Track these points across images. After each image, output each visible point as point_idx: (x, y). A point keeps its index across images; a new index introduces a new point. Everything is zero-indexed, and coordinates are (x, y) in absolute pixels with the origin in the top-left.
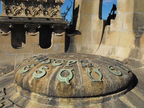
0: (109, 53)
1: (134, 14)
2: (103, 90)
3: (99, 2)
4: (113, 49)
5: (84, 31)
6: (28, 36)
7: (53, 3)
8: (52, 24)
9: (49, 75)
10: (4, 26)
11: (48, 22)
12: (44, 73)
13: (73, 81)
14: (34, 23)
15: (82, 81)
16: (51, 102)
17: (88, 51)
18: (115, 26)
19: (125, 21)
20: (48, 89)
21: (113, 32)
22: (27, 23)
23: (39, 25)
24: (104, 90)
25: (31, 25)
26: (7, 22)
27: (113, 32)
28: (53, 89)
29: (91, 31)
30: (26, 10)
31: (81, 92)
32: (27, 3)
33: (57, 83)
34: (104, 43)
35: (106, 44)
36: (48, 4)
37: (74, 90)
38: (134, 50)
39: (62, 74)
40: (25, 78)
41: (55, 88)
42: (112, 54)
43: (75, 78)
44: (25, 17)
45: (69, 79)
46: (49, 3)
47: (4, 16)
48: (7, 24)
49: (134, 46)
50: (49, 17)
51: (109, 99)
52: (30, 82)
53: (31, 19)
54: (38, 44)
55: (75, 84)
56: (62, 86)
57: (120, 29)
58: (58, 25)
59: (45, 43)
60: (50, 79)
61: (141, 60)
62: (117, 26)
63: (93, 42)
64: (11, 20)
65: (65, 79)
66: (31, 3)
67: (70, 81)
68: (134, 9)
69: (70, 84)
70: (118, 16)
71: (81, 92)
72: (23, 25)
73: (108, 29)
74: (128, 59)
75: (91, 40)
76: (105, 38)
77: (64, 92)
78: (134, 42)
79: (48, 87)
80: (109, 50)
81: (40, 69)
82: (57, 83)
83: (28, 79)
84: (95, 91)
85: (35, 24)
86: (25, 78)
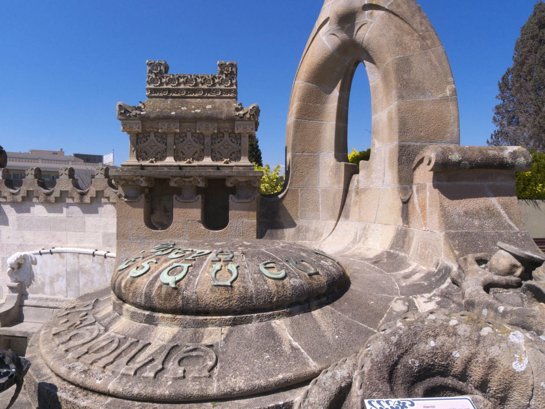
0: (354, 239)
1: (400, 146)
2: (231, 301)
3: (335, 123)
4: (364, 229)
5: (301, 190)
9: (152, 272)
10: (130, 183)
11: (218, 174)
13: (183, 283)
14: (191, 177)
15: (196, 284)
16: (148, 318)
17: (311, 236)
18: (369, 176)
19: (387, 165)
20: (143, 294)
21: (365, 190)
22: (175, 177)
23: (199, 180)
24: (235, 301)
25: (184, 181)
26: (136, 176)
27: (365, 190)
28: (150, 295)
29: (319, 190)
31: (191, 301)
32: (177, 136)
33: (157, 284)
34: (347, 217)
35: (350, 218)
36: (221, 135)
37: (180, 297)
38: (401, 230)
40: (119, 279)
41: (154, 293)
42: (359, 241)
43: (189, 277)
44: (171, 164)
45: (177, 279)
46: (223, 133)
47: (132, 163)
48: (136, 180)
49: (400, 222)
51: (249, 321)
52: (123, 284)
53: (288, 164)
54: (199, 221)
55: (184, 287)
58: (240, 180)
59: (215, 219)
60: (151, 279)
61: (408, 254)
62: (374, 175)
63: (322, 213)
64: (144, 172)
65: (171, 280)
66: (186, 136)
67: (177, 282)
68: (400, 137)
69: (175, 289)
70: (375, 151)
71: (191, 301)
73: (356, 183)
74: (388, 253)
75: (318, 210)
76: (350, 206)
77: (165, 299)
78: (400, 211)
79: (144, 292)
80: (357, 233)
82: (157, 284)
83: (123, 278)
84: (216, 301)
85: (192, 179)
86: (119, 279)
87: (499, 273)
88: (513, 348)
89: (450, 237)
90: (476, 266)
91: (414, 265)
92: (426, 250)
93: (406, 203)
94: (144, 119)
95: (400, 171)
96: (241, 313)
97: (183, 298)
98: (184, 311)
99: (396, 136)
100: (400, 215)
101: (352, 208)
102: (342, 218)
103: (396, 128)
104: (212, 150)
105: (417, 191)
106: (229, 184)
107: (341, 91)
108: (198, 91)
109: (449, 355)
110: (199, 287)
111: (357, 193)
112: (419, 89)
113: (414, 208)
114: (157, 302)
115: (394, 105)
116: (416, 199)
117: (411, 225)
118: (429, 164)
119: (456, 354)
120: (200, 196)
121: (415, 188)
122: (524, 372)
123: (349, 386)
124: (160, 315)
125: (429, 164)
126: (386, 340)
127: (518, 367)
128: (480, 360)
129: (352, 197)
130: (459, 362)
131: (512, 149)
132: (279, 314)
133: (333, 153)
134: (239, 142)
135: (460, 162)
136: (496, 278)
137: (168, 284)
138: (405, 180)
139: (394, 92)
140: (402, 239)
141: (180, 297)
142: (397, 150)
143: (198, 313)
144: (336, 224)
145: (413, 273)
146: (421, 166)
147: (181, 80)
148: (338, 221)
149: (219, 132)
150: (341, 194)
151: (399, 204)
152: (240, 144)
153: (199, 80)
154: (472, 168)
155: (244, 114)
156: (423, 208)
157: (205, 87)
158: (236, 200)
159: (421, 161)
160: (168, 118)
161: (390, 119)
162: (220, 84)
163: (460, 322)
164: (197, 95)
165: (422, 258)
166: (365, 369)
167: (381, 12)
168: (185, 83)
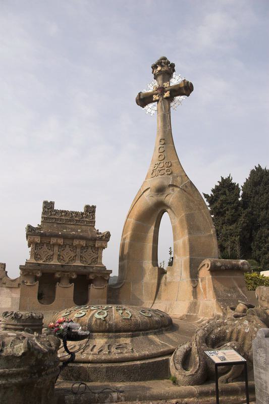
3: (152, 244)
6: (59, 288)
7: (92, 247)
8: (90, 273)
11: (85, 270)
12: (84, 313)
13: (107, 318)
18: (172, 275)
19: (183, 269)
27: (170, 282)
30: (59, 255)
34: (160, 298)
35: (26, 226)
37: (107, 324)
39: (99, 313)
50: (64, 264)
51: (138, 335)
56: (98, 321)
57: (179, 279)
62: (175, 274)
69: (104, 320)
72: (54, 274)
74: (187, 315)
76: (161, 292)
81: (81, 312)
82: (94, 319)
85: (69, 273)
87: (240, 313)
88: (245, 326)
89: (218, 300)
90: (231, 310)
91: (202, 318)
92: (207, 309)
93: (195, 288)
94: (42, 236)
95: (191, 272)
96: (136, 331)
97: (109, 324)
98: (109, 331)
99: (188, 254)
100: (192, 294)
101: (162, 294)
102: (157, 299)
103: (188, 249)
104: (81, 256)
105: (201, 281)
106: (91, 277)
107: (155, 227)
108: (73, 220)
109: (225, 332)
110: (116, 320)
111: (165, 285)
112: (199, 229)
113: (200, 290)
114: (94, 327)
115: (186, 237)
116: (200, 285)
117: (199, 299)
118: (208, 267)
119: (227, 331)
120: (73, 284)
121: (200, 280)
122: (248, 332)
123: (190, 350)
124: (96, 334)
125: (208, 267)
126: (204, 329)
127: (247, 331)
128: (235, 331)
129: (162, 285)
130: (228, 334)
131: (242, 261)
132: (151, 333)
133: (151, 261)
134: (97, 252)
135: (221, 266)
136: (239, 314)
137: (100, 319)
138: (194, 275)
139: (186, 231)
140: (194, 306)
141: (107, 324)
142: (188, 260)
143: (117, 331)
144: (154, 303)
145: (202, 321)
146: (203, 268)
147: (63, 214)
148: (155, 299)
149: (86, 246)
150: (156, 285)
151: (190, 289)
152: (98, 253)
153: (73, 215)
154: (226, 269)
155: (102, 237)
156: (205, 289)
157: (77, 219)
158: (95, 287)
159: (204, 265)
160: (57, 236)
161: (184, 243)
162: (86, 218)
163: (228, 321)
164: (72, 223)
165: (205, 314)
166: (197, 340)
167: (179, 189)
168: (65, 215)
